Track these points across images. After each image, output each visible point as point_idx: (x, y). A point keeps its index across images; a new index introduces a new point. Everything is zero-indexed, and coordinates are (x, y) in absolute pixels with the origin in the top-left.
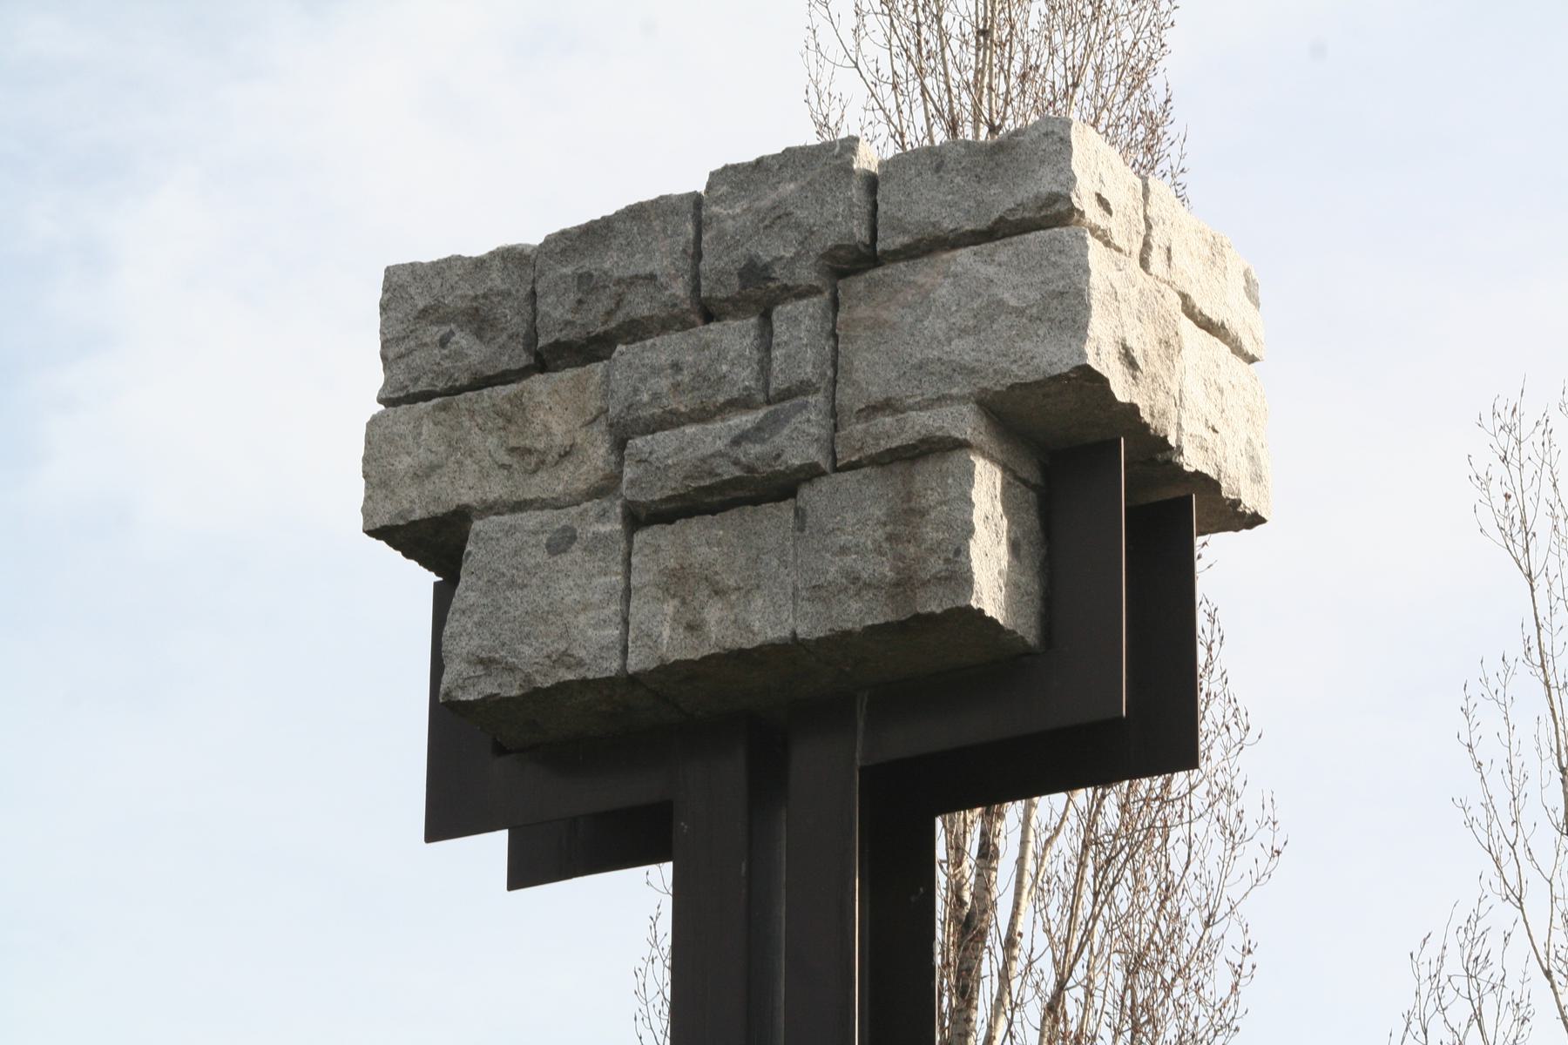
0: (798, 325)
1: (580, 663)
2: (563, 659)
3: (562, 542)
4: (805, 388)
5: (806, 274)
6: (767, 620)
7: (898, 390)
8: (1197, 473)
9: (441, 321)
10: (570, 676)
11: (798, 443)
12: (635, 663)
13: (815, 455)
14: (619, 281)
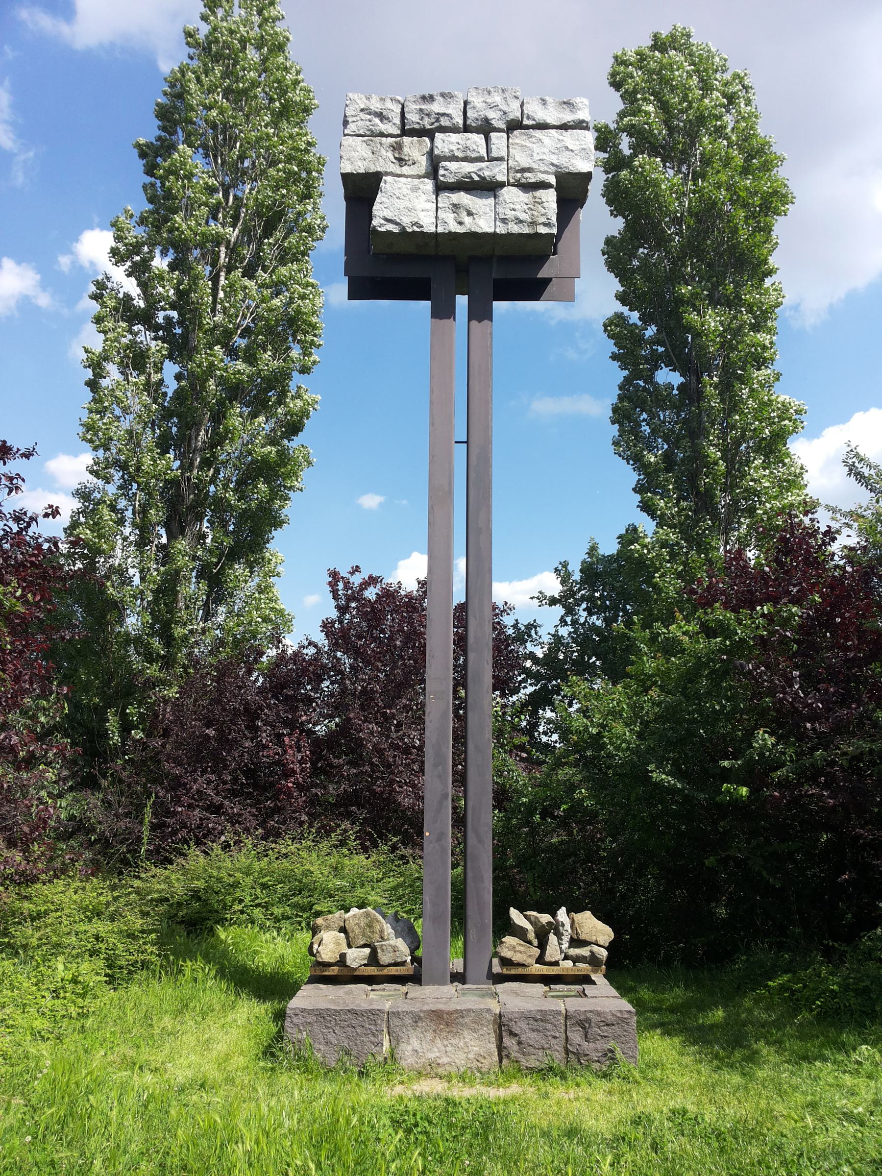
0: (498, 140)
1: (422, 227)
2: (416, 224)
3: (415, 189)
4: (500, 159)
5: (502, 125)
6: (485, 224)
7: (534, 166)
8: (409, 556)
9: (370, 114)
10: (418, 230)
11: (499, 172)
12: (440, 230)
13: (505, 179)
14: (438, 114)
